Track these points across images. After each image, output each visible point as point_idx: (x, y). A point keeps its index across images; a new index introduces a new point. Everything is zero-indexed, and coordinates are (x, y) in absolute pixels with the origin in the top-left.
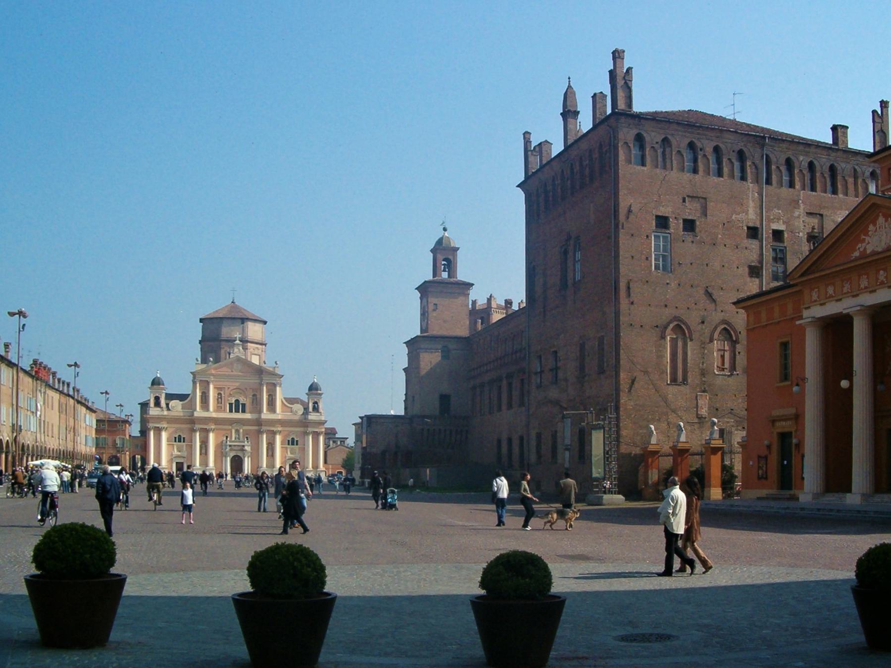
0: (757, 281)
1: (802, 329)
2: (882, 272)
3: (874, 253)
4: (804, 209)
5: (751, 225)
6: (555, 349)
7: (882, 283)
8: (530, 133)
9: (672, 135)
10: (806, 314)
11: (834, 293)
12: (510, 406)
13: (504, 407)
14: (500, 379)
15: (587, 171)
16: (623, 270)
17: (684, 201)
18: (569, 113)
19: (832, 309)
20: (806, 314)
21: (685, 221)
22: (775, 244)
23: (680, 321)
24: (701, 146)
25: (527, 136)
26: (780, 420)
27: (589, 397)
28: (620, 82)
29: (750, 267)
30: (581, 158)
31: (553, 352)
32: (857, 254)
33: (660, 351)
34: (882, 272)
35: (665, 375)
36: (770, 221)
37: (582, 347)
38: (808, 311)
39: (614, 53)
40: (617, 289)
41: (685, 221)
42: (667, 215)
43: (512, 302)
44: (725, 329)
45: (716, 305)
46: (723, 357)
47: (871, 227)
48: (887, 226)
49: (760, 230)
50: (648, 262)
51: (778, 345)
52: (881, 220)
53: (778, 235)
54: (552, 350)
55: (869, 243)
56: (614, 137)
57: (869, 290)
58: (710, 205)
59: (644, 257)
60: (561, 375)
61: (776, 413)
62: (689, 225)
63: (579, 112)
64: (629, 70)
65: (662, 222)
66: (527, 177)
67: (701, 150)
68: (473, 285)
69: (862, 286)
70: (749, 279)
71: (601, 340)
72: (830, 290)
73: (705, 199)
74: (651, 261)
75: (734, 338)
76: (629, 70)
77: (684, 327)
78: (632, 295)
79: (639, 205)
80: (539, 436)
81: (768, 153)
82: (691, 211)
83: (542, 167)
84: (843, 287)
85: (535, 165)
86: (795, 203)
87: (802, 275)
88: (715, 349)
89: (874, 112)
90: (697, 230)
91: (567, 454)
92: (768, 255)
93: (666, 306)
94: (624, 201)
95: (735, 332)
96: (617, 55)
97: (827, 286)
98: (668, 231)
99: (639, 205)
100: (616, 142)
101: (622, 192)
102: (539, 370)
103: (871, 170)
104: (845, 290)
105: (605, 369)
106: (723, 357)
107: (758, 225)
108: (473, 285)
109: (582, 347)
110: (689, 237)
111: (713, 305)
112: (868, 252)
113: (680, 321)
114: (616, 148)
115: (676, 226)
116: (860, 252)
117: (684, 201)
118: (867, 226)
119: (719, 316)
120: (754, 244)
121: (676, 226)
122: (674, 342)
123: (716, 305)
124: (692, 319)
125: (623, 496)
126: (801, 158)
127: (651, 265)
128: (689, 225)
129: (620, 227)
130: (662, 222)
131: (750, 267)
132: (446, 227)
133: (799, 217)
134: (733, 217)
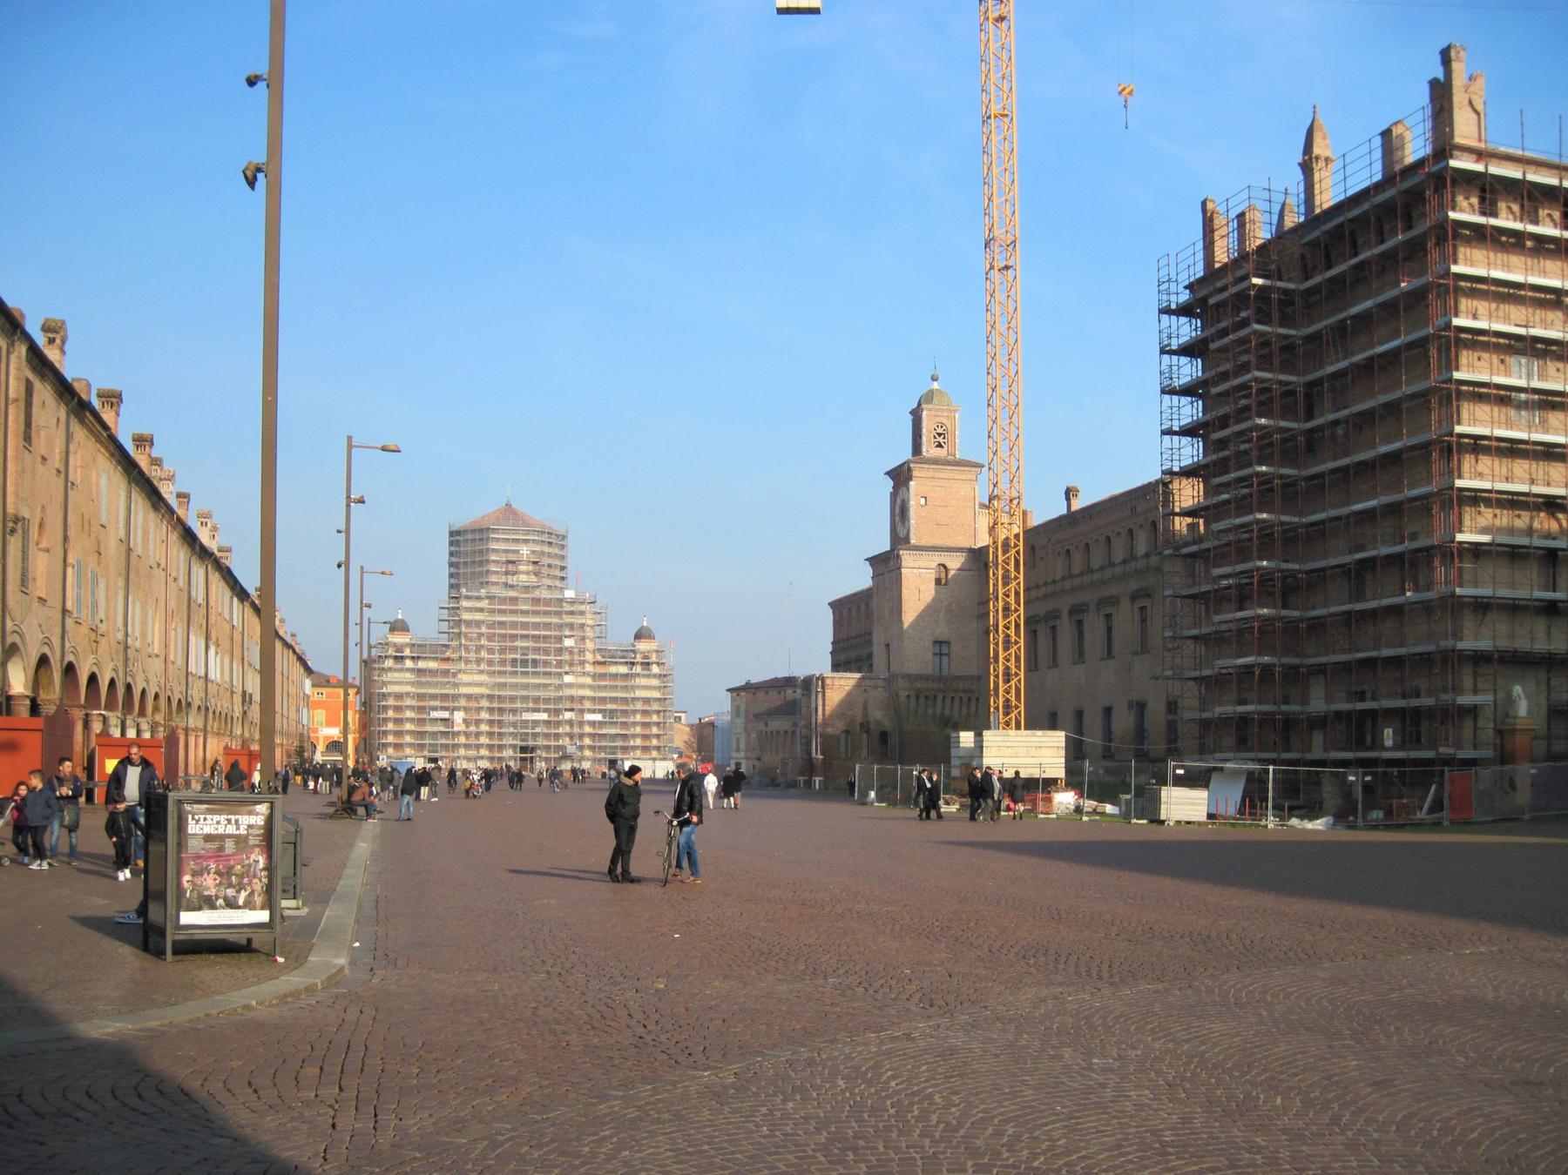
12: (1080, 656)
85: (1223, 254)
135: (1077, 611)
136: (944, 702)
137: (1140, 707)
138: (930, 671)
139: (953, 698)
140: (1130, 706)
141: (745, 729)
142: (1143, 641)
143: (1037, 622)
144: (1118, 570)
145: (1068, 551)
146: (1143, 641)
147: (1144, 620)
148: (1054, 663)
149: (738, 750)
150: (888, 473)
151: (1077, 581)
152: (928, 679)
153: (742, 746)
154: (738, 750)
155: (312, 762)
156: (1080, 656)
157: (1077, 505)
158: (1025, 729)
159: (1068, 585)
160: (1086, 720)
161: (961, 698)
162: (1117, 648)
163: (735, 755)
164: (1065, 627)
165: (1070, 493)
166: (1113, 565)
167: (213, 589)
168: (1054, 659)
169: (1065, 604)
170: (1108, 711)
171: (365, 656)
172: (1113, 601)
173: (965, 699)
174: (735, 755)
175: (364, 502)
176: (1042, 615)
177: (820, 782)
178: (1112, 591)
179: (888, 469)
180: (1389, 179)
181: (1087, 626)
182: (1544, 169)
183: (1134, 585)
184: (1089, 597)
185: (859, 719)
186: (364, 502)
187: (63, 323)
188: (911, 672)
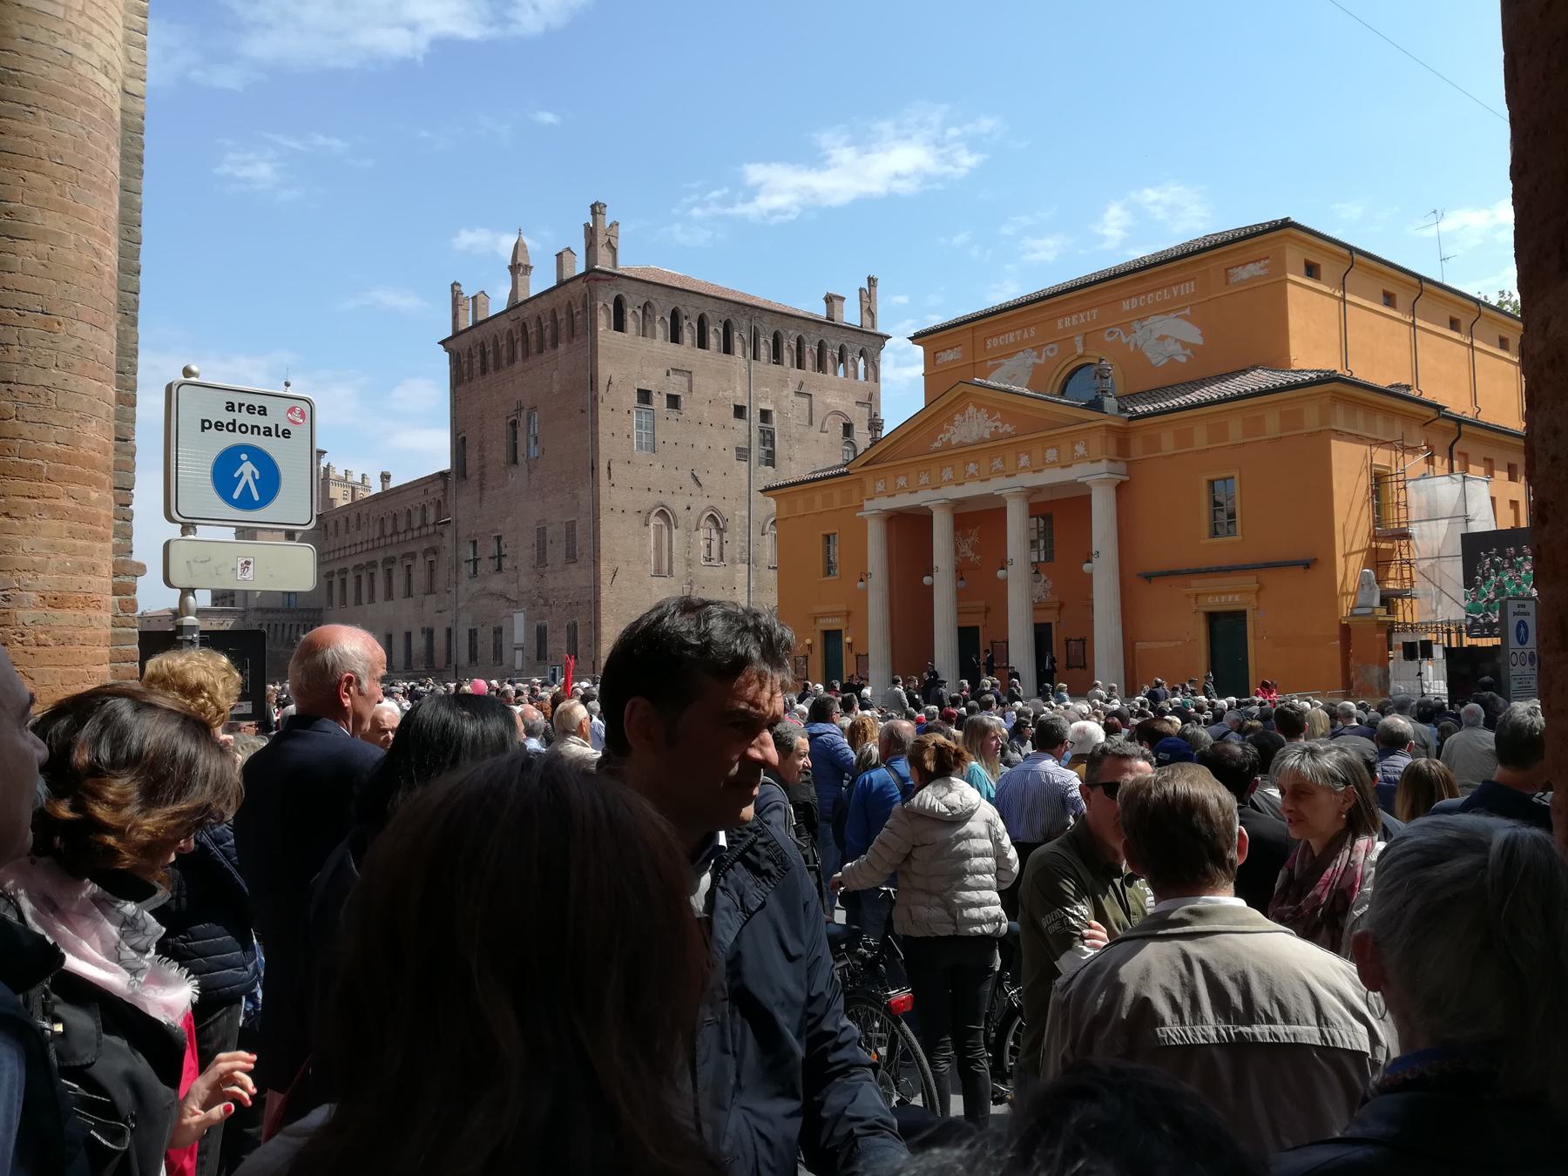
0: (745, 464)
1: (864, 522)
2: (971, 465)
3: (961, 445)
4: (792, 387)
5: (739, 403)
6: (499, 534)
7: (972, 476)
8: (458, 284)
9: (656, 299)
10: (868, 505)
11: (907, 484)
12: (389, 596)
13: (365, 600)
14: (373, 564)
15: (548, 333)
16: (603, 448)
17: (668, 374)
18: (518, 268)
19: (903, 501)
20: (868, 505)
21: (669, 396)
22: (763, 425)
23: (663, 506)
24: (687, 314)
25: (456, 288)
26: (823, 617)
27: (553, 590)
28: (601, 239)
29: (738, 449)
30: (539, 318)
31: (495, 537)
32: (937, 444)
33: (644, 539)
34: (971, 465)
35: (649, 565)
36: (758, 399)
37: (541, 533)
38: (870, 502)
39: (593, 207)
40: (594, 469)
41: (669, 396)
42: (649, 389)
43: (390, 476)
44: (711, 515)
45: (702, 490)
46: (709, 546)
47: (958, 417)
48: (979, 416)
49: (748, 408)
50: (630, 440)
51: (821, 538)
52: (971, 409)
53: (765, 415)
54: (493, 535)
55: (954, 433)
56: (591, 297)
57: (931, 486)
58: (696, 380)
59: (625, 435)
60: (506, 563)
61: (817, 609)
62: (674, 401)
63: (531, 267)
64: (615, 225)
65: (645, 396)
66: (457, 334)
67: (686, 318)
68: (325, 452)
69: (945, 478)
70: (736, 462)
71: (571, 527)
72: (902, 481)
73: (690, 372)
74: (633, 439)
75: (722, 527)
76: (615, 225)
77: (669, 513)
78: (612, 476)
79: (620, 376)
80: (473, 634)
81: (757, 325)
82: (677, 385)
83: (476, 324)
84: (919, 478)
85: (467, 321)
86: (783, 383)
87: (864, 465)
88: (702, 537)
89: (861, 290)
90: (682, 407)
91: (519, 653)
92: (756, 435)
93: (649, 489)
94: (605, 370)
95: (722, 518)
96: (596, 209)
97: (897, 477)
98: (651, 407)
99: (620, 376)
100: (593, 303)
101: (601, 361)
102: (472, 558)
103: (860, 349)
104: (922, 482)
105: (577, 558)
106: (709, 546)
107: (746, 403)
108: (325, 452)
109: (541, 533)
110: (673, 414)
111: (699, 489)
112: (953, 443)
113: (663, 506)
114: (594, 311)
115: (659, 402)
116: (943, 442)
117: (668, 374)
118: (953, 416)
119: (706, 503)
120: (741, 424)
121: (659, 402)
122: (659, 528)
123: (702, 490)
124: (677, 505)
125: (601, 708)
126: (790, 332)
127: (633, 445)
128: (674, 401)
129: (600, 400)
130: (645, 396)
131: (738, 449)
132: (289, 381)
133: (787, 396)
134: (720, 394)
136: (291, 629)
137: (429, 633)
138: (280, 606)
139: (298, 625)
140: (423, 632)
143: (362, 569)
144: (416, 534)
145: (382, 518)
147: (432, 570)
148: (372, 599)
151: (389, 541)
152: (268, 611)
155: (1335, 778)
156: (389, 596)
157: (393, 484)
158: (1416, 643)
160: (394, 640)
161: (305, 625)
162: (414, 591)
164: (380, 574)
165: (385, 477)
166: (398, 533)
167: (864, 316)
169: (379, 556)
170: (408, 635)
172: (413, 556)
173: (556, 552)
176: (364, 564)
178: (410, 548)
180: (562, 283)
181: (395, 574)
188: (263, 606)
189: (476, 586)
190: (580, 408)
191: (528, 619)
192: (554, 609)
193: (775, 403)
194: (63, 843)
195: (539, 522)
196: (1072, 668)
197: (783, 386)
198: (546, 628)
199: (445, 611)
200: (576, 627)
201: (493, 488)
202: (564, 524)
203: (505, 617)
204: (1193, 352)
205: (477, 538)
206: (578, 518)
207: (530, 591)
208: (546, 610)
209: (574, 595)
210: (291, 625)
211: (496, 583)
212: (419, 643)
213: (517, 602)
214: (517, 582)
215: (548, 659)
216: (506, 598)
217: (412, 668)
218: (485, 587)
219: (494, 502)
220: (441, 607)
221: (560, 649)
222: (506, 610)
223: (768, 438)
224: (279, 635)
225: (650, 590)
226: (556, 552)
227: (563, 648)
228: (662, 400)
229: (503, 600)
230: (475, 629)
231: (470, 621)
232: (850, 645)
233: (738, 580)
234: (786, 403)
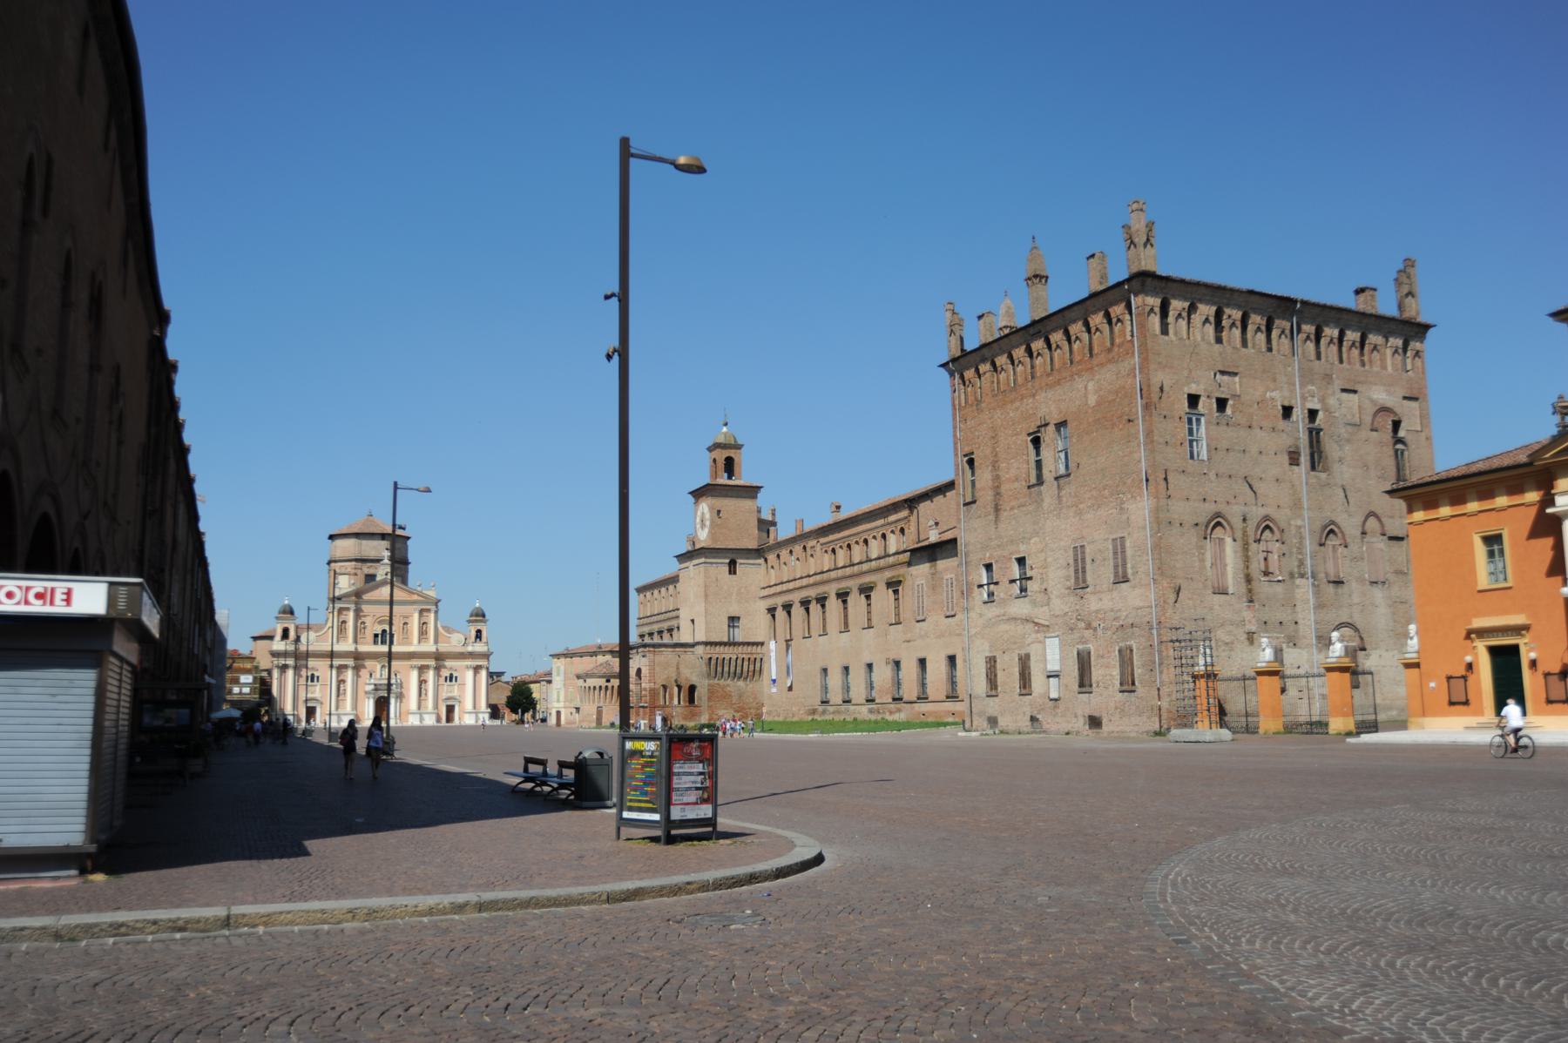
12: (846, 627)
27: (1097, 612)
80: (992, 662)
102: (394, 649)
119: (1262, 512)
128: (1222, 404)
130: (1193, 400)
135: (843, 596)
141: (564, 685)
142: (897, 615)
146: (897, 615)
149: (558, 701)
150: (691, 493)
153: (562, 698)
154: (558, 701)
156: (846, 627)
159: (833, 575)
163: (556, 705)
168: (846, 624)
171: (331, 596)
173: (1099, 574)
174: (556, 705)
175: (430, 491)
177: (645, 724)
179: (691, 490)
182: (1456, 474)
183: (888, 574)
184: (812, 593)
185: (674, 676)
186: (430, 491)
187: (177, 361)
189: (992, 611)
190: (1126, 417)
191: (1062, 645)
192: (1100, 632)
193: (1322, 400)
194: (236, 713)
195: (1075, 540)
196: (1448, 681)
197: (1329, 384)
198: (1089, 653)
199: (915, 640)
200: (1131, 651)
201: (1012, 509)
202: (1110, 541)
203: (1032, 643)
204: (1334, 417)
205: (993, 562)
206: (1129, 534)
207: (1066, 614)
208: (1088, 633)
209: (1127, 616)
210: (755, 659)
211: (1021, 608)
212: (883, 675)
213: (1048, 626)
214: (1048, 605)
215: (1094, 685)
216: (1034, 622)
217: (927, 698)
218: (1005, 612)
219: (1013, 522)
220: (909, 636)
221: (1111, 675)
222: (1034, 636)
223: (1315, 435)
224: (739, 669)
225: (1211, 609)
226: (1099, 574)
227: (1114, 673)
228: (1211, 404)
229: (1031, 625)
230: (995, 657)
231: (987, 648)
232: (1533, 664)
233: (1298, 597)
234: (1332, 401)
